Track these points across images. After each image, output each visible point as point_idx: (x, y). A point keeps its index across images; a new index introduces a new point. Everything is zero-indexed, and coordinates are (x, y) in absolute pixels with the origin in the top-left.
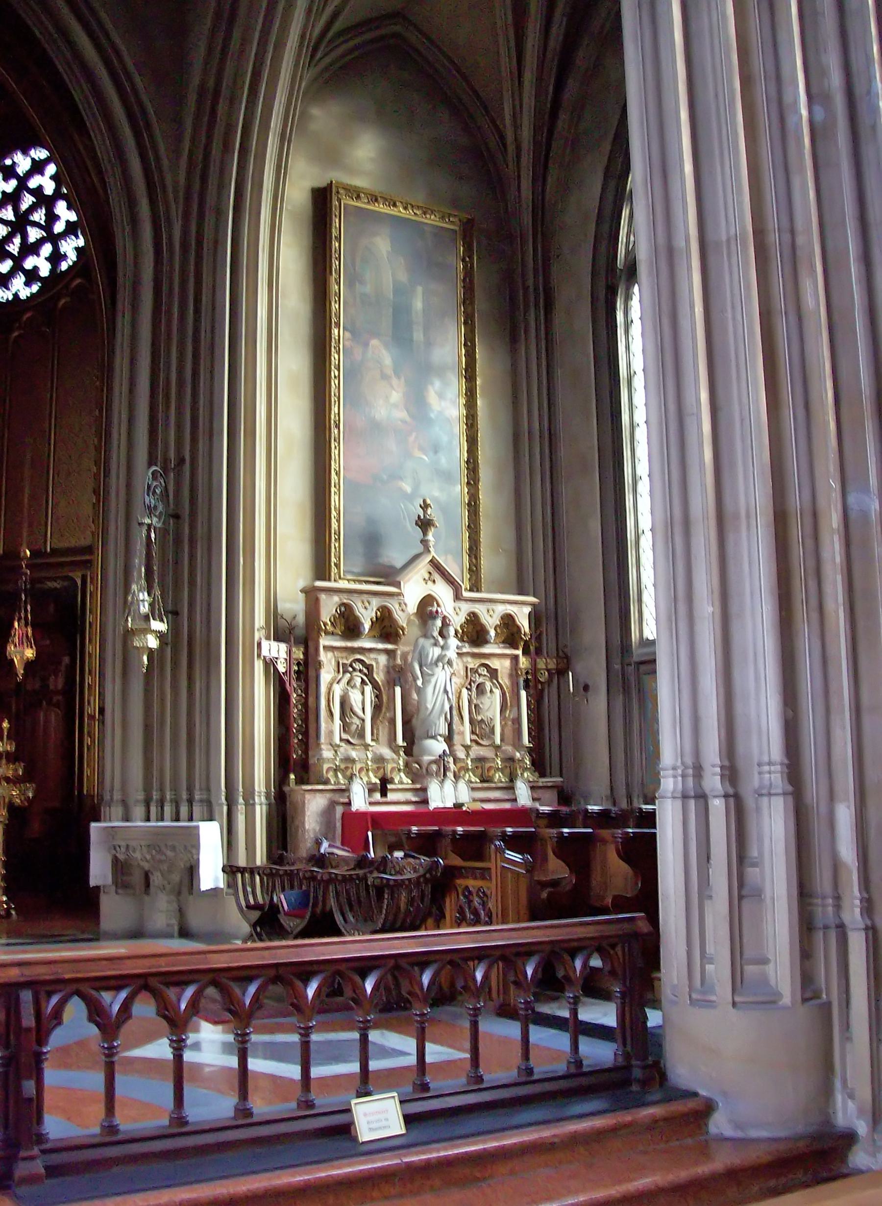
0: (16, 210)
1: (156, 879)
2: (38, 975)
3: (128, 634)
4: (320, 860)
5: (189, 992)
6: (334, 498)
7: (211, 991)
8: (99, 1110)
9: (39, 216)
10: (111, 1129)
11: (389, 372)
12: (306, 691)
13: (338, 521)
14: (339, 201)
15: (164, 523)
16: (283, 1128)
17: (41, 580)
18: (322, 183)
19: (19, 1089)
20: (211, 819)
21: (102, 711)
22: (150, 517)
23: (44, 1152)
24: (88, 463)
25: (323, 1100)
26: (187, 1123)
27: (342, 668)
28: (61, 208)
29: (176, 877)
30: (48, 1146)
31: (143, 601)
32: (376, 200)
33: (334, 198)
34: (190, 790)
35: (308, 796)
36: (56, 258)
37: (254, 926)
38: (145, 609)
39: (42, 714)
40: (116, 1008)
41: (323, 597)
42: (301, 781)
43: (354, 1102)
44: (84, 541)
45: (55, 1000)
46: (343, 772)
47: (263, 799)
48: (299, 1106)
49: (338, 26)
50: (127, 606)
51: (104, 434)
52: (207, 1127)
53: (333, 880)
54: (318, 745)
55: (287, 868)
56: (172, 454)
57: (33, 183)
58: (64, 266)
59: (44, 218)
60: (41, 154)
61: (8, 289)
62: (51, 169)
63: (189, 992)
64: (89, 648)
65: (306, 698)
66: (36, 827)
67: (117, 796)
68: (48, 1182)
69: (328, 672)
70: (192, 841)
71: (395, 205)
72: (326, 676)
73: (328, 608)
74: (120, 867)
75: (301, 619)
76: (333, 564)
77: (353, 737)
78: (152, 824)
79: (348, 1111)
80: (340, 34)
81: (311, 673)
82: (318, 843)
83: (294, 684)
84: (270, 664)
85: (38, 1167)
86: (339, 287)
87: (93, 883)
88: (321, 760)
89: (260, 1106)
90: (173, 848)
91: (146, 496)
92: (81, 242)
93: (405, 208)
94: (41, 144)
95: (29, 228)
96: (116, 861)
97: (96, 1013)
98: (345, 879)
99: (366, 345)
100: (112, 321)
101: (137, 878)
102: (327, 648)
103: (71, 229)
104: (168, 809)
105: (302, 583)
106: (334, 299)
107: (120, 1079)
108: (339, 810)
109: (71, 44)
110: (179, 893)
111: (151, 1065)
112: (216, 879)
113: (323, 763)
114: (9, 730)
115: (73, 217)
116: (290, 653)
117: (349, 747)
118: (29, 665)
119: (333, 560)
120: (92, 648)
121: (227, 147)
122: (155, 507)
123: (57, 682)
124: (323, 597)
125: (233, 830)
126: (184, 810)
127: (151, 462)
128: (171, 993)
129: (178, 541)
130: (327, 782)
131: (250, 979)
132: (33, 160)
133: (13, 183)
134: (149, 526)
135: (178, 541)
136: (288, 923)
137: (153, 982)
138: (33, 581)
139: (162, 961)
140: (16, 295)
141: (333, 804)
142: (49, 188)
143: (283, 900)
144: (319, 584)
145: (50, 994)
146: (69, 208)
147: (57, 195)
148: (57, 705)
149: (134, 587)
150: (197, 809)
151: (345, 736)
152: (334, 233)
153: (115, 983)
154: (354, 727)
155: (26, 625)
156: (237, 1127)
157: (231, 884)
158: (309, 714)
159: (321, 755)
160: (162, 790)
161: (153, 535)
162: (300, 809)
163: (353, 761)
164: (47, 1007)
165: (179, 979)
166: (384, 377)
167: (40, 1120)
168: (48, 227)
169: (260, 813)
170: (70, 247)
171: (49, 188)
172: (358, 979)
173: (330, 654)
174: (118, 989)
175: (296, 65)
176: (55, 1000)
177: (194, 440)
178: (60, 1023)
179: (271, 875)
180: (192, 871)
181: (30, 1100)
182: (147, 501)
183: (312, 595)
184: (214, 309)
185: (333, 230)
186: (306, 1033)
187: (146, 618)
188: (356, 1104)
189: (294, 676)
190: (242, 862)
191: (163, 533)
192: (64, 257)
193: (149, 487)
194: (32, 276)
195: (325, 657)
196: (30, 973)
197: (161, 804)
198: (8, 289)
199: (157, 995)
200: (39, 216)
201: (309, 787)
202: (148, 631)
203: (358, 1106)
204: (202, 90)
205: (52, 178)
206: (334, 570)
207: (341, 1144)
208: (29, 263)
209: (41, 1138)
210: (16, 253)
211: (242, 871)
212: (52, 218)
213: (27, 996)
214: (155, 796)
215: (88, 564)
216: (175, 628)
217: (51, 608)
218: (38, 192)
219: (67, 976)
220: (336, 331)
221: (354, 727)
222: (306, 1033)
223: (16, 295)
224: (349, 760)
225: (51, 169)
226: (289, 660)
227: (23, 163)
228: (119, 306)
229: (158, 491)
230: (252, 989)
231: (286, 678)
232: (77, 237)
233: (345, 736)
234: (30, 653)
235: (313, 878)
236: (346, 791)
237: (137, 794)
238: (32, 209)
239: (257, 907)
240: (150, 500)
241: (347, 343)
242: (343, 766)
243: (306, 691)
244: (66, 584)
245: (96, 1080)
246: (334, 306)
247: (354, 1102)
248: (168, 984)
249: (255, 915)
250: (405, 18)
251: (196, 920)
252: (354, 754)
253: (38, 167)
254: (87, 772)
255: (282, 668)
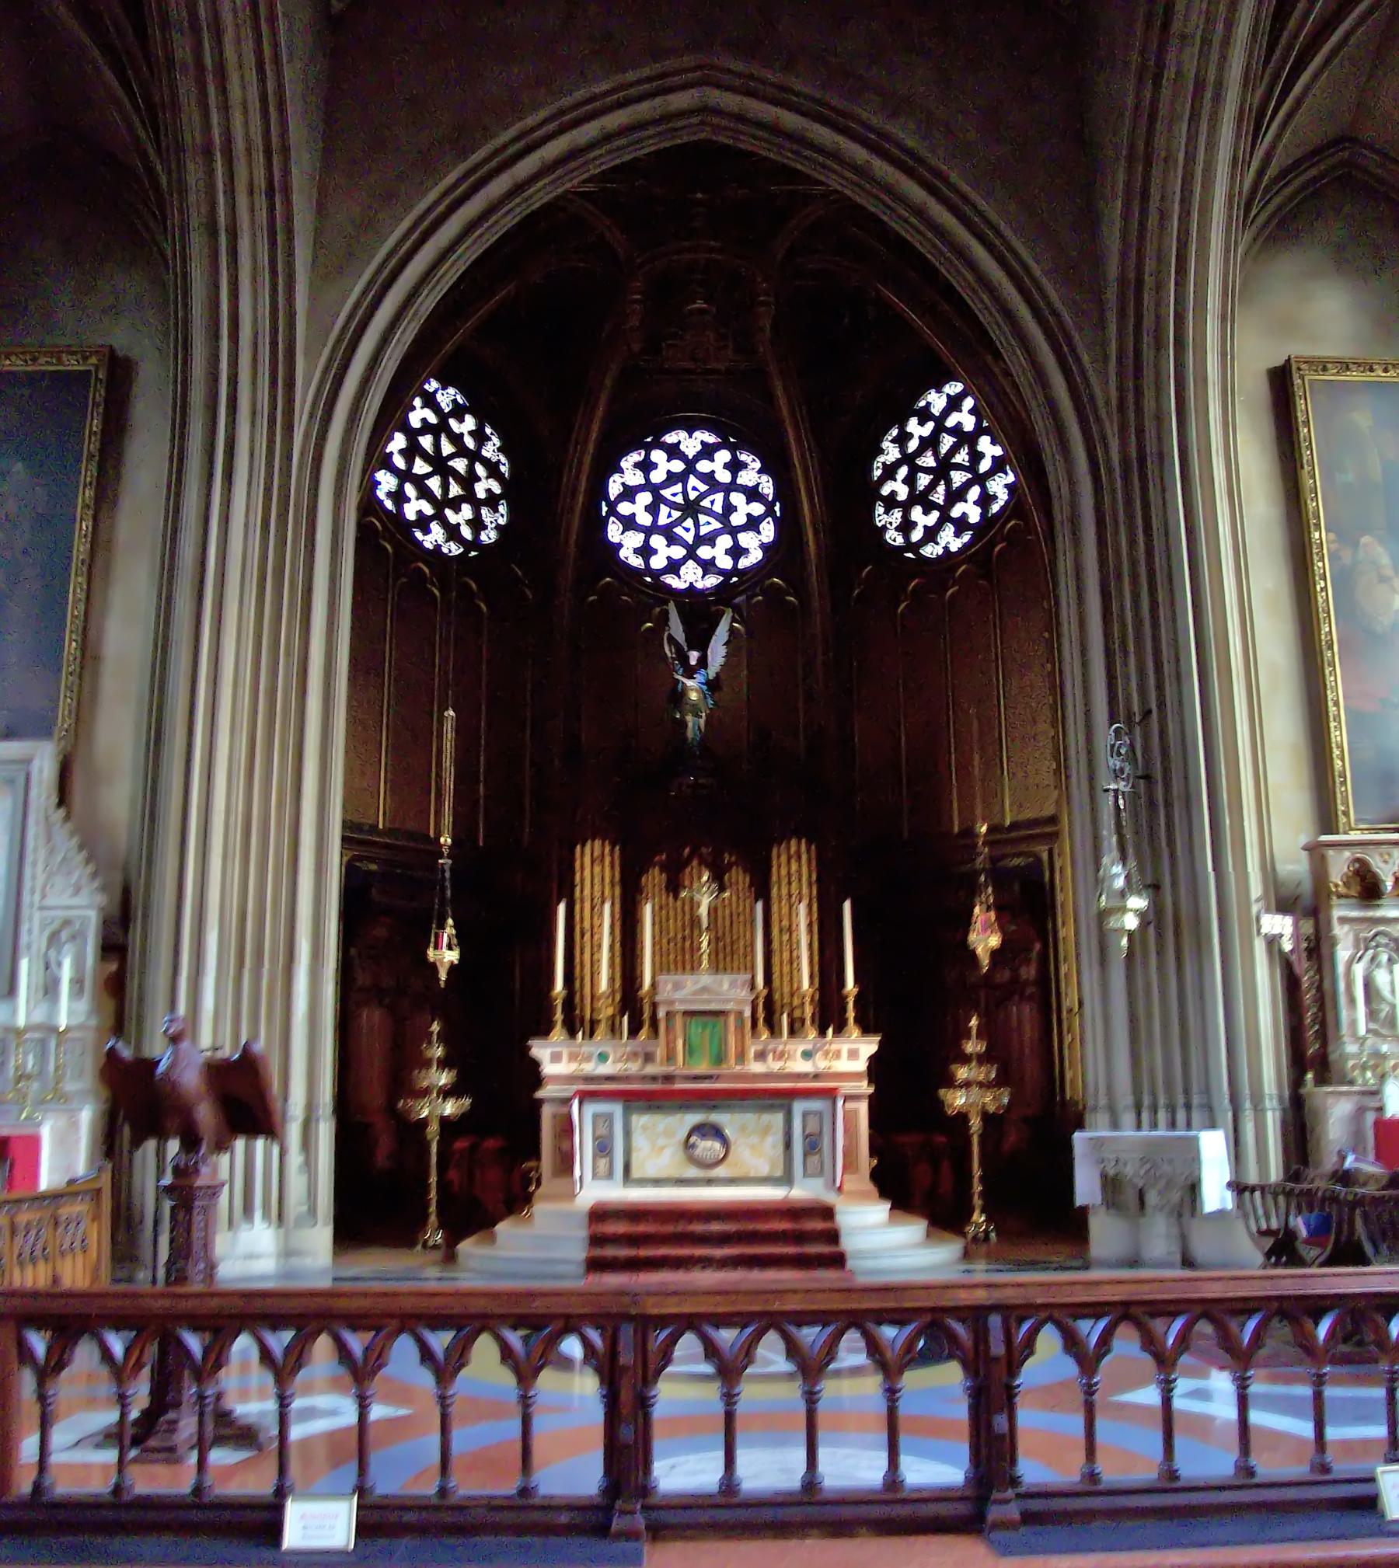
0: (936, 454)
1: (1152, 1198)
2: (1007, 1298)
3: (1103, 915)
4: (1345, 1178)
5: (1178, 1324)
6: (1334, 734)
7: (1205, 1328)
8: (1080, 1457)
9: (962, 457)
10: (1092, 1477)
11: (1389, 572)
12: (1319, 971)
13: (1343, 760)
14: (1302, 378)
15: (1133, 787)
16: (1291, 1494)
17: (1003, 857)
18: (1279, 361)
19: (989, 1425)
20: (1212, 1125)
21: (1081, 1004)
22: (1116, 782)
23: (1018, 1495)
24: (1044, 727)
25: (1341, 1467)
26: (1178, 1478)
27: (1363, 945)
28: (984, 444)
29: (1175, 1196)
30: (1022, 1490)
31: (1117, 874)
32: (1348, 369)
33: (1295, 376)
34: (1187, 1092)
35: (1330, 1101)
36: (985, 500)
37: (1268, 1255)
38: (1120, 883)
39: (1015, 1009)
40: (1094, 1340)
41: (1331, 853)
42: (1322, 1080)
43: (1380, 1469)
44: (1048, 810)
45: (1026, 1326)
46: (1375, 1068)
47: (1275, 1103)
48: (1312, 1470)
49: (1272, 171)
50: (1099, 883)
51: (1057, 689)
52: (1202, 1484)
53: (1358, 1202)
54: (1339, 1038)
55: (1305, 1186)
56: (1136, 708)
57: (950, 422)
58: (995, 508)
59: (967, 458)
60: (954, 388)
61: (937, 544)
62: (968, 403)
63: (1178, 1324)
64: (1062, 934)
65: (1321, 981)
66: (1012, 1139)
67: (1103, 1101)
68: (1023, 1530)
69: (1345, 949)
70: (1191, 1154)
71: (1372, 370)
72: (1343, 954)
73: (1339, 867)
74: (1111, 1185)
75: (1307, 887)
76: (1340, 813)
77: (1383, 1026)
78: (1144, 1133)
79: (1372, 1480)
80: (1275, 180)
81: (1325, 950)
82: (1343, 1158)
83: (1306, 965)
84: (1272, 941)
85: (1013, 1511)
86: (1314, 478)
87: (1079, 1201)
88: (1345, 1057)
89: (1267, 1466)
90: (1171, 1162)
91: (1109, 758)
92: (1011, 478)
93: (1386, 370)
94: (952, 377)
95: (952, 473)
96: (1104, 1176)
97: (1072, 1343)
98: (1376, 1201)
99: (1356, 544)
100: (1053, 562)
101: (1130, 1196)
102: (1343, 920)
103: (998, 466)
104: (1162, 1116)
105: (1304, 839)
106: (1309, 496)
107: (1100, 1424)
108: (1370, 1118)
109: (972, 265)
110: (1180, 1215)
111: (1138, 1411)
112: (1223, 1199)
113: (1347, 1059)
114: (979, 1026)
115: (998, 451)
116: (1296, 925)
117: (1378, 1040)
118: (995, 954)
119: (1341, 808)
120: (1067, 931)
121: (1159, 345)
122: (1122, 770)
123: (1029, 972)
124: (1331, 853)
125: (1242, 1140)
126: (1181, 1116)
127: (1113, 718)
128: (1158, 1325)
129: (1152, 804)
130: (1351, 1083)
131: (1250, 1313)
132: (948, 395)
133: (930, 426)
134: (1116, 791)
135: (1152, 804)
136: (1310, 1253)
137: (1133, 1310)
138: (994, 860)
139: (1146, 1288)
140: (946, 548)
141: (1360, 1111)
142: (969, 423)
143: (1300, 1225)
144: (1324, 838)
145: (1021, 1320)
146: (993, 443)
147: (979, 431)
148: (1031, 998)
149: (1105, 860)
150: (1196, 1116)
151: (1373, 1026)
152: (1301, 418)
153: (1094, 1310)
154: (1383, 1015)
155: (988, 909)
156: (1240, 1487)
157: (1240, 1205)
158: (1325, 1001)
159: (1343, 1050)
160: (1154, 1094)
161: (1121, 802)
162: (1320, 1115)
163: (1384, 1057)
164: (1018, 1333)
165: (1167, 1309)
166: (1383, 579)
167: (1013, 1461)
168: (972, 467)
169: (1272, 1121)
170: (998, 486)
171: (969, 423)
172: (1380, 1319)
173: (1346, 928)
174: (1098, 1317)
175: (1228, 231)
176: (1026, 1326)
177: (1160, 687)
178: (1031, 1353)
179: (1288, 1194)
180: (1194, 1189)
181: (1003, 1436)
182: (1111, 764)
183: (1316, 852)
184: (1167, 534)
185: (1299, 414)
186: (1319, 1381)
187: (1123, 894)
188: (1383, 1472)
189: (1304, 955)
190: (1252, 1177)
191: (1135, 795)
192: (995, 498)
193: (1113, 746)
194: (961, 525)
195: (1340, 931)
196: (997, 1296)
197: (1154, 1110)
198: (937, 544)
199: (1139, 1325)
200: (962, 457)
201: (1330, 1089)
202: (1124, 910)
203: (1387, 1477)
204: (1122, 281)
205: (971, 412)
206: (1342, 819)
207: (1367, 1521)
208: (956, 512)
209: (1015, 1481)
210: (941, 502)
211: (1253, 1190)
212: (976, 457)
213: (995, 1321)
214: (1146, 1101)
215: (1054, 836)
216: (1156, 906)
217: (1016, 887)
218: (957, 430)
219: (1039, 1301)
220: (1317, 535)
221: (1383, 1015)
222: (1319, 1381)
223: (946, 548)
224: (1381, 1057)
225: (968, 403)
226: (1296, 936)
227: (936, 401)
228: (1059, 545)
229: (1123, 751)
230: (1251, 1324)
231: (1293, 958)
232: (1006, 474)
233: (1373, 1026)
234: (995, 941)
235: (1334, 1199)
236: (1376, 1093)
237: (1125, 1099)
238: (954, 450)
239: (1268, 1233)
240: (1116, 763)
241: (1333, 546)
242: (1371, 1063)
243: (1319, 971)
244: (1031, 859)
245: (1075, 1423)
246: (1312, 505)
247: (1380, 1469)
248: (1154, 1315)
249: (1269, 1242)
250: (1353, 140)
251: (1201, 1249)
252: (1385, 1048)
253: (954, 404)
254: (1068, 1075)
255: (1287, 946)
